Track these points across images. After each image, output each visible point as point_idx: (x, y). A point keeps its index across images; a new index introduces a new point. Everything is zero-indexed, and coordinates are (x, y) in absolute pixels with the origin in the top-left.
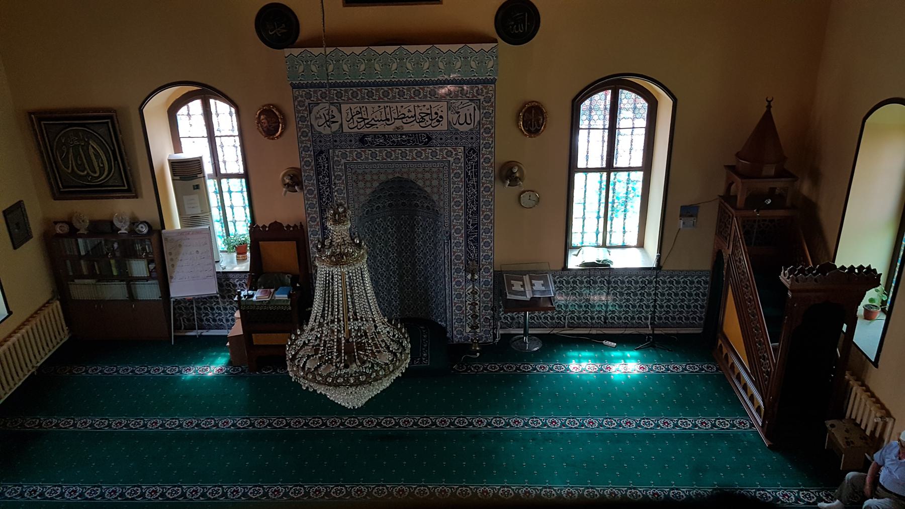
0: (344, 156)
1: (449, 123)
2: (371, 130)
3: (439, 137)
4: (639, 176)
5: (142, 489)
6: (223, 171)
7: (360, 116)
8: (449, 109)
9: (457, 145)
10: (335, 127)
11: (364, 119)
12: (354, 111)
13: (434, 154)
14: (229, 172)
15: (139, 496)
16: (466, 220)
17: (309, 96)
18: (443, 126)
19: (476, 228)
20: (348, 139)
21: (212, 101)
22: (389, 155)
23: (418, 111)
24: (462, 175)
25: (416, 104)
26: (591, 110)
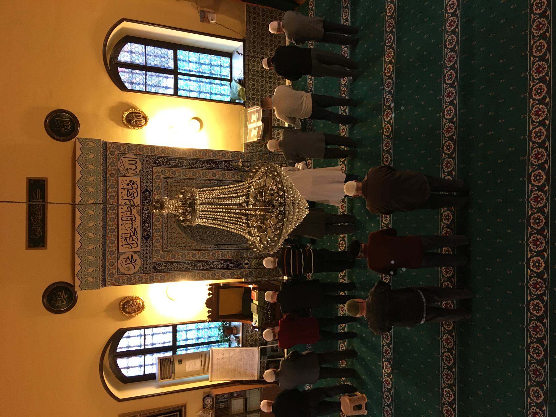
0: (157, 251)
1: (135, 176)
2: (139, 232)
3: (145, 184)
4: (181, 54)
5: (385, 391)
6: (171, 344)
7: (128, 239)
8: (124, 176)
9: (151, 172)
10: (136, 257)
11: (131, 236)
12: (124, 243)
13: (158, 188)
14: (171, 339)
15: (390, 393)
16: (206, 169)
17: (112, 275)
18: (137, 180)
19: (212, 161)
20: (145, 248)
21: (118, 350)
22: (158, 220)
23: (126, 197)
24: (174, 169)
25: (120, 199)
26: (132, 83)
